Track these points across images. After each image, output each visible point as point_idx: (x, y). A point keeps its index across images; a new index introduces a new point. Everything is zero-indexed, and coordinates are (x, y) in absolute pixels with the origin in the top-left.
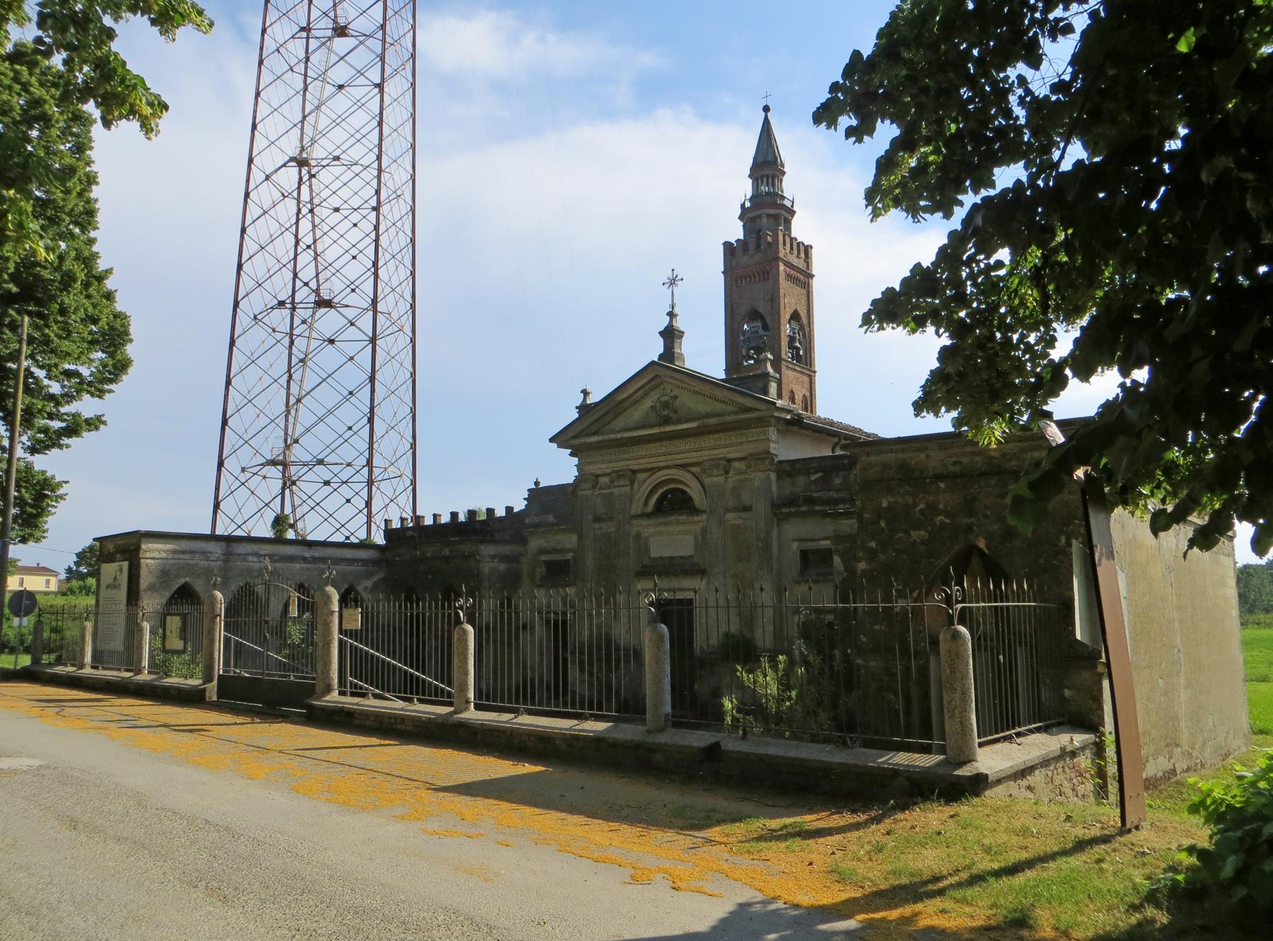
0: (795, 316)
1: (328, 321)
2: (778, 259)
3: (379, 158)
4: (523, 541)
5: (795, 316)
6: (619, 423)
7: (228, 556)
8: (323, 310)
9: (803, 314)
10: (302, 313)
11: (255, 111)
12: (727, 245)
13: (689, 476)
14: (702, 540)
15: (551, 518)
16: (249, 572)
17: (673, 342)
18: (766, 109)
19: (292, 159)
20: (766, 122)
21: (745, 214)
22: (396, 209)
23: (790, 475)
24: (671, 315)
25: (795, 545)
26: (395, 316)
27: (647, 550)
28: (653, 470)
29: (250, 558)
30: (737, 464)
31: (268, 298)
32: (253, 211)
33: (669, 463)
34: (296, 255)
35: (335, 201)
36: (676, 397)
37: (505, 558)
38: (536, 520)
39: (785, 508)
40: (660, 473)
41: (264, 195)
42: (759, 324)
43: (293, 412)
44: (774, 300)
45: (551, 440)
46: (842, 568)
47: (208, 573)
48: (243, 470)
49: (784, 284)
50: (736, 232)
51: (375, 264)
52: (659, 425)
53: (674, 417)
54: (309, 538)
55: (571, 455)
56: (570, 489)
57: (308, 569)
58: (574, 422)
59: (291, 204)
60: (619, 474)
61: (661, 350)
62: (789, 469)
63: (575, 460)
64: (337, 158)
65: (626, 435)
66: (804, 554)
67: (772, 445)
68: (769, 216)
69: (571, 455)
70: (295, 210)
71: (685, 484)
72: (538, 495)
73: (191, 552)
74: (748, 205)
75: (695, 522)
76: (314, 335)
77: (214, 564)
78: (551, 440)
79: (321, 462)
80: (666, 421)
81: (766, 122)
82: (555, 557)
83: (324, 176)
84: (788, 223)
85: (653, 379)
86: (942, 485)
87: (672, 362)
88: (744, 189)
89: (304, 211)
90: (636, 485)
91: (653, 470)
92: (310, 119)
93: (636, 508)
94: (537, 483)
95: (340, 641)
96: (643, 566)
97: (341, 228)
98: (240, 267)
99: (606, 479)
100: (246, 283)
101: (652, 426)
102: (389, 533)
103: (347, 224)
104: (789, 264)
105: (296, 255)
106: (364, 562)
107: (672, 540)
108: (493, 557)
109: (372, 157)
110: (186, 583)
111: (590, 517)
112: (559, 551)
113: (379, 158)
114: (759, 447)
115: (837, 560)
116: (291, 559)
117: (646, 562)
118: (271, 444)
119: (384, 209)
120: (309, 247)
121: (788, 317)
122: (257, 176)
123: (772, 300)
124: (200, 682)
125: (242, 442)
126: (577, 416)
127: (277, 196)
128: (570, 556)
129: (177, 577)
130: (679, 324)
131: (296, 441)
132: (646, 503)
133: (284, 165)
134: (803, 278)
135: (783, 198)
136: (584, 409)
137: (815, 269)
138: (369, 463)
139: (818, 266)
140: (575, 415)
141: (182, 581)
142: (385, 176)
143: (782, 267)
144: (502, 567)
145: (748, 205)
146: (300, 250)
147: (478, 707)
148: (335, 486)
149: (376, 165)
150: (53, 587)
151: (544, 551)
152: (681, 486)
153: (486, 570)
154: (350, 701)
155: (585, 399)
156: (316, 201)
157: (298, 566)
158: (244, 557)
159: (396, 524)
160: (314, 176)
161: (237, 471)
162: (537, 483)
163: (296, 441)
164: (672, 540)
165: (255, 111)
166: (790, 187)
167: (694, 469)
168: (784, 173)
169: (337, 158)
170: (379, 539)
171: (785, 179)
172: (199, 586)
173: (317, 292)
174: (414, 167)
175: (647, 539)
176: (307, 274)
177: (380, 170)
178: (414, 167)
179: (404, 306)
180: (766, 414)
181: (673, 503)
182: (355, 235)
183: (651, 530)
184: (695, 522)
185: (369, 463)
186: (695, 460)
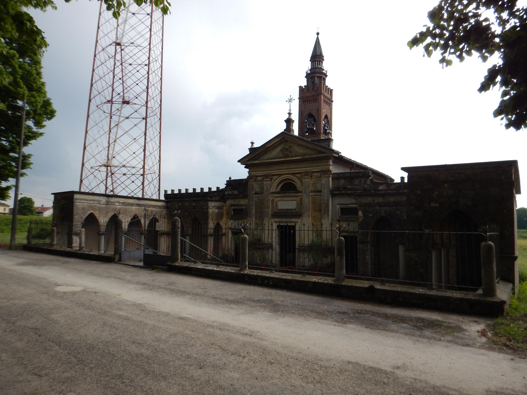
0: (326, 117)
1: (127, 110)
2: (321, 94)
3: (150, 44)
4: (225, 202)
5: (326, 117)
6: (267, 156)
7: (107, 203)
8: (125, 105)
9: (329, 116)
10: (115, 107)
11: (99, 21)
12: (301, 87)
13: (295, 178)
14: (300, 204)
15: (236, 192)
16: (115, 209)
17: (290, 125)
18: (318, 34)
19: (114, 42)
20: (318, 38)
21: (308, 76)
22: (155, 66)
23: (337, 178)
24: (290, 114)
25: (338, 206)
26: (154, 109)
27: (277, 206)
28: (280, 175)
29: (116, 204)
30: (316, 174)
31: (102, 98)
32: (98, 63)
33: (287, 172)
34: (113, 83)
35: (130, 61)
36: (291, 146)
37: (218, 208)
38: (230, 193)
39: (335, 193)
40: (283, 176)
41: (102, 56)
42: (312, 119)
43: (112, 146)
44: (319, 111)
45: (239, 161)
46: (362, 215)
47: (100, 209)
48: (92, 168)
49: (323, 104)
50: (304, 83)
51: (147, 88)
52: (285, 158)
53: (290, 154)
54: (119, 194)
55: (245, 167)
56: (245, 181)
57: (138, 209)
58: (248, 155)
59: (112, 60)
60: (266, 176)
61: (285, 128)
62: (337, 177)
63: (248, 170)
64: (133, 43)
65: (270, 161)
66: (342, 209)
67: (331, 167)
68: (318, 77)
69: (245, 167)
70: (113, 63)
71: (294, 181)
72: (231, 183)
73: (94, 200)
74: (309, 72)
75: (298, 196)
76: (122, 115)
77: (102, 206)
78: (239, 161)
79: (124, 166)
80: (287, 156)
81: (318, 38)
82: (238, 208)
83: (126, 50)
84: (324, 79)
85: (282, 139)
86: (446, 185)
87: (290, 132)
88: (308, 66)
89: (118, 64)
90: (273, 180)
91: (280, 175)
92: (121, 27)
93: (273, 189)
94: (230, 178)
95: (182, 240)
96: (275, 212)
97: (133, 72)
98: (92, 85)
99: (261, 178)
100: (94, 92)
101: (281, 158)
102: (166, 195)
103: (135, 71)
104: (325, 96)
105: (113, 83)
106: (160, 207)
107: (288, 204)
108: (214, 207)
109: (147, 43)
110: (92, 213)
111: (253, 192)
112: (239, 205)
113: (150, 44)
114: (325, 168)
115: (360, 213)
116: (132, 205)
117: (275, 210)
118: (103, 159)
119: (151, 65)
120: (120, 79)
121: (324, 117)
122: (99, 48)
123: (318, 110)
124: (113, 253)
125: (92, 156)
126: (248, 153)
127: (107, 57)
128: (244, 207)
129: (88, 210)
130: (291, 112)
131: (114, 157)
132: (277, 188)
133: (111, 45)
134: (329, 102)
135: (323, 70)
136: (251, 149)
137: (334, 99)
138: (144, 167)
139: (335, 98)
140: (248, 152)
141: (90, 212)
142: (152, 52)
143: (322, 97)
144: (217, 211)
145: (309, 72)
146: (115, 80)
147: (249, 268)
148: (129, 176)
149: (148, 47)
150: (7, 211)
151: (232, 205)
152: (292, 182)
153: (211, 212)
154: (186, 264)
155: (252, 145)
156: (123, 60)
157: (135, 207)
158: (113, 204)
159: (169, 192)
160: (123, 50)
161: (89, 168)
162: (230, 178)
163: (114, 157)
164: (288, 204)
165: (99, 21)
166: (326, 65)
167: (298, 175)
168: (323, 60)
169: (133, 43)
170: (162, 198)
171: (324, 62)
172: (97, 214)
173: (123, 99)
174: (162, 49)
175: (276, 203)
176: (119, 89)
177: (150, 49)
178: (162, 49)
179: (157, 105)
180: (330, 154)
181: (288, 188)
182: (138, 75)
183: (279, 199)
184: (298, 196)
185: (144, 167)
186: (298, 172)
